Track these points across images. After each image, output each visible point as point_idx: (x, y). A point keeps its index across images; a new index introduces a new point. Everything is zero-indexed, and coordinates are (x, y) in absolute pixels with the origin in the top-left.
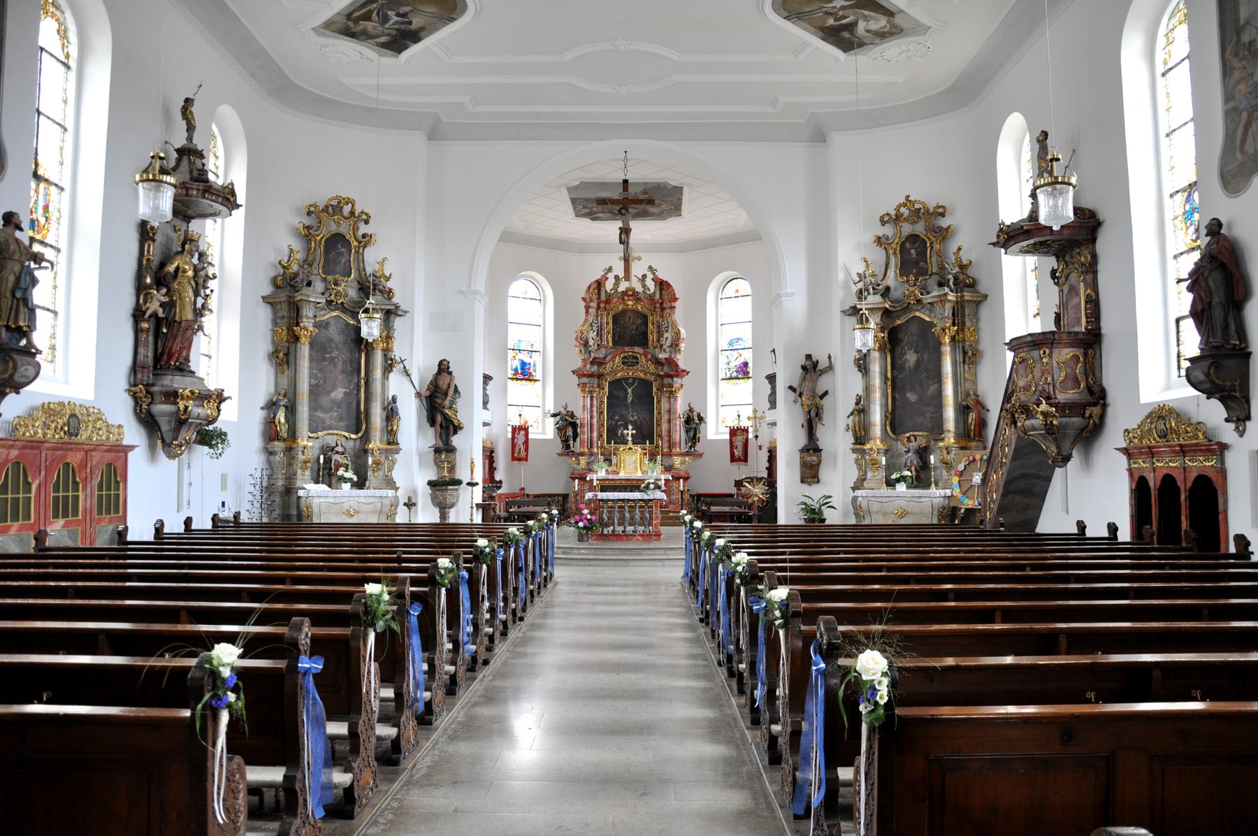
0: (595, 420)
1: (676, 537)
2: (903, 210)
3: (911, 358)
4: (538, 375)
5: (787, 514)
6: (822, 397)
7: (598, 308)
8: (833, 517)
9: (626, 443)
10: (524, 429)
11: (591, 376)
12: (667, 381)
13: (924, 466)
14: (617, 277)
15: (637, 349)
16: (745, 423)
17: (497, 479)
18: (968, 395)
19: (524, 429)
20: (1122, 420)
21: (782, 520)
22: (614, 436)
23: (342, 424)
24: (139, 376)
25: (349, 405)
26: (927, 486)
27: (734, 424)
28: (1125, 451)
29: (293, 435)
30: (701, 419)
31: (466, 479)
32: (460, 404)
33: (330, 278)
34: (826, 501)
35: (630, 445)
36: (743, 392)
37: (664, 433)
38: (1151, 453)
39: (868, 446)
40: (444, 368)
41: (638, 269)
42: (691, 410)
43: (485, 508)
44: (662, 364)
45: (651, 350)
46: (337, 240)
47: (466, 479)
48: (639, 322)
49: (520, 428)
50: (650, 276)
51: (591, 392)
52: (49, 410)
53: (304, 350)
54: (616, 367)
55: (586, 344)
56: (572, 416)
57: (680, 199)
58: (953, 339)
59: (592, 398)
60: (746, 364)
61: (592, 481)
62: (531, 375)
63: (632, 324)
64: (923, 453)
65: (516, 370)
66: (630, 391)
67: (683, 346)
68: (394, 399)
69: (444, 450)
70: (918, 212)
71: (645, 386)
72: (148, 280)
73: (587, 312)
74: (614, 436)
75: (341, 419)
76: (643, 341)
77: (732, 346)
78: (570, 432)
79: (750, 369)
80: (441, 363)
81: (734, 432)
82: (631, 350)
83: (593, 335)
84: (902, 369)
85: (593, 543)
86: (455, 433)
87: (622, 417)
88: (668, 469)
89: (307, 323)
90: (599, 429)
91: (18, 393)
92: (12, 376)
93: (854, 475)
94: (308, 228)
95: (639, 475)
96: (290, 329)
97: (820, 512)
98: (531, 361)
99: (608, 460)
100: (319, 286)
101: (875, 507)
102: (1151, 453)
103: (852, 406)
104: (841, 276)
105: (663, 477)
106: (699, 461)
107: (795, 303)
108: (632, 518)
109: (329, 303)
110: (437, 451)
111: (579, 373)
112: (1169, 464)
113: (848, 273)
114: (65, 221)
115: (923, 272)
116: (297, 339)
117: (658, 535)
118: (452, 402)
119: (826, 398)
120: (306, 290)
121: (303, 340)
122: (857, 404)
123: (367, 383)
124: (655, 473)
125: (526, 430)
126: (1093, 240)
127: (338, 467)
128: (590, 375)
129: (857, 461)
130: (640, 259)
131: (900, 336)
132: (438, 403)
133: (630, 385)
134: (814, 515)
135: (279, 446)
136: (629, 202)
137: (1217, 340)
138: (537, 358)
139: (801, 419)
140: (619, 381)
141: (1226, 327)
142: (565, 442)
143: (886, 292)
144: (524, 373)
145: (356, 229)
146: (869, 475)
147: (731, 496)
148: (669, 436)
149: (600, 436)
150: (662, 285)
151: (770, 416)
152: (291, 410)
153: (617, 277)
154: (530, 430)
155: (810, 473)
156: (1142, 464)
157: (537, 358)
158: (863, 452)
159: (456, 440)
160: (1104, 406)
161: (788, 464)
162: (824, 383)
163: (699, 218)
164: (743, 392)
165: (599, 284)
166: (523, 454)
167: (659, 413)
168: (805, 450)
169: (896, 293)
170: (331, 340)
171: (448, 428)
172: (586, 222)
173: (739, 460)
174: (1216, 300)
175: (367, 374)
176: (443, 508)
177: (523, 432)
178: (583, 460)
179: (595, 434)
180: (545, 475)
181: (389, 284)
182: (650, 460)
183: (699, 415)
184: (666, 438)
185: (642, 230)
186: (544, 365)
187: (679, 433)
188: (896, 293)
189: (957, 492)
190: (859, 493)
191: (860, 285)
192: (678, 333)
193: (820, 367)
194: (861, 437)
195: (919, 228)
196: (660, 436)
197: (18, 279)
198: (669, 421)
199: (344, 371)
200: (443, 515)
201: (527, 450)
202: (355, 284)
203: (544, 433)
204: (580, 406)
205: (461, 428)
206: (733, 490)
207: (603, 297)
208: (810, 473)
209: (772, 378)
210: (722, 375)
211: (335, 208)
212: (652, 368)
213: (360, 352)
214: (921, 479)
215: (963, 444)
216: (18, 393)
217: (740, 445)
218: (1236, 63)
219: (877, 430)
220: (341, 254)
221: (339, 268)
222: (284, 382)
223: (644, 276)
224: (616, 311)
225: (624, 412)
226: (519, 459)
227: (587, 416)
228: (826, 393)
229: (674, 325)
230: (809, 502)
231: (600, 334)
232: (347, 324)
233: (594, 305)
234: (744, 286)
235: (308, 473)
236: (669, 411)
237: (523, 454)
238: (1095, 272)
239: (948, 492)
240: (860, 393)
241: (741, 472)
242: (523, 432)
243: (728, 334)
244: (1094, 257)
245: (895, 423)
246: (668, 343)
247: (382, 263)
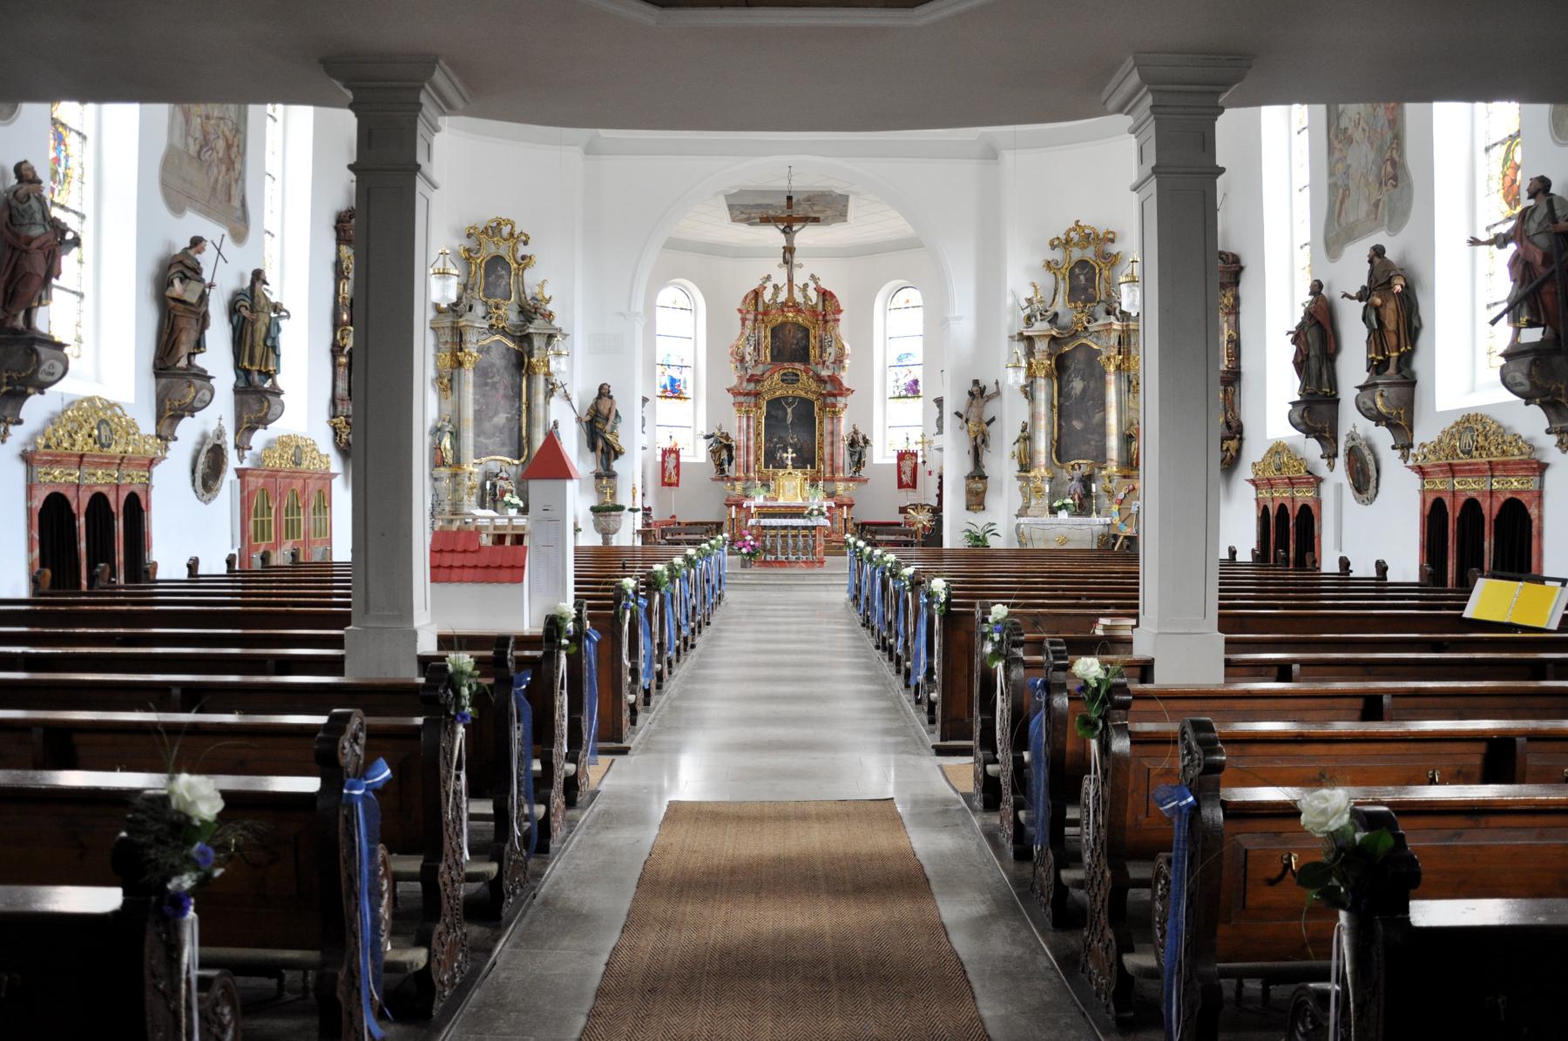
1: (841, 566)
2: (1072, 234)
3: (1077, 385)
4: (688, 392)
5: (952, 539)
6: (988, 424)
8: (995, 543)
9: (785, 467)
10: (674, 452)
11: (748, 394)
12: (830, 400)
13: (1087, 494)
14: (776, 287)
15: (797, 365)
16: (912, 448)
18: (1132, 424)
19: (674, 452)
20: (1254, 452)
21: (947, 544)
22: (772, 460)
23: (505, 449)
24: (340, 408)
25: (511, 429)
26: (1089, 514)
27: (902, 447)
28: (1253, 482)
29: (458, 461)
30: (866, 442)
31: (628, 505)
32: (621, 429)
33: (491, 302)
34: (991, 529)
35: (790, 469)
36: (914, 412)
37: (827, 457)
38: (1270, 484)
39: (1032, 474)
41: (800, 278)
43: (645, 535)
45: (812, 366)
46: (496, 262)
47: (628, 505)
49: (671, 451)
50: (812, 285)
52: (284, 443)
53: (468, 376)
54: (774, 386)
55: (742, 360)
56: (727, 437)
57: (846, 206)
58: (1118, 368)
60: (916, 382)
61: (749, 508)
63: (792, 338)
64: (1087, 481)
67: (847, 362)
68: (556, 424)
69: (605, 474)
70: (1089, 238)
71: (806, 405)
72: (345, 317)
74: (772, 460)
75: (503, 445)
76: (803, 355)
78: (724, 455)
79: (920, 387)
80: (601, 387)
82: (791, 368)
83: (750, 349)
84: (1069, 396)
85: (756, 570)
86: (616, 457)
87: (780, 438)
88: (831, 495)
89: (471, 348)
91: (42, 393)
92: (36, 371)
93: (1018, 502)
94: (469, 250)
95: (799, 501)
96: (453, 355)
97: (985, 539)
98: (681, 377)
99: (766, 485)
100: (480, 310)
101: (1037, 534)
102: (1270, 484)
103: (1018, 433)
104: (1009, 300)
105: (825, 504)
106: (864, 488)
107: (963, 327)
108: (795, 545)
109: (491, 326)
110: (598, 476)
111: (735, 392)
112: (1282, 494)
113: (1016, 300)
114: (89, 178)
115: (1091, 299)
116: (460, 364)
117: (822, 562)
118: (614, 427)
120: (468, 316)
121: (467, 365)
123: (529, 408)
124: (818, 500)
125: (677, 452)
126: (1237, 283)
127: (503, 493)
128: (747, 393)
129: (1021, 488)
130: (801, 266)
131: (1068, 363)
132: (599, 426)
133: (789, 405)
134: (978, 540)
135: (444, 472)
136: (790, 213)
137: (1312, 388)
138: (687, 375)
139: (967, 446)
140: (778, 399)
141: (1320, 376)
143: (1054, 319)
144: (674, 391)
145: (515, 250)
146: (1033, 502)
147: (899, 524)
150: (825, 295)
151: (938, 441)
152: (456, 436)
153: (776, 287)
154: (682, 453)
155: (976, 500)
156: (1265, 494)
158: (1027, 480)
159: (616, 466)
160: (1241, 439)
161: (954, 491)
162: (990, 410)
163: (866, 223)
164: (914, 412)
165: (757, 294)
166: (674, 479)
169: (1064, 319)
170: (492, 365)
172: (744, 227)
173: (908, 486)
174: (1312, 353)
175: (529, 399)
176: (606, 534)
178: (739, 486)
179: (752, 458)
180: (697, 501)
181: (549, 307)
184: (828, 463)
185: (806, 236)
186: (696, 381)
187: (843, 457)
188: (1064, 319)
189: (1116, 519)
190: (1022, 520)
191: (1028, 311)
192: (842, 348)
194: (1026, 466)
195: (1089, 254)
196: (822, 459)
197: (268, 330)
198: (832, 444)
199: (505, 396)
200: (606, 540)
202: (516, 308)
203: (695, 456)
204: (736, 427)
206: (900, 518)
207: (761, 309)
208: (976, 500)
209: (939, 402)
211: (494, 230)
212: (814, 386)
213: (521, 376)
214: (1084, 506)
215: (1126, 472)
216: (42, 393)
218: (1336, 144)
219: (1042, 458)
220: (501, 277)
221: (499, 291)
222: (448, 408)
223: (806, 285)
224: (774, 323)
225: (783, 434)
226: (670, 485)
227: (743, 438)
230: (973, 529)
231: (757, 349)
232: (508, 349)
233: (751, 316)
234: (914, 296)
235: (473, 499)
237: (674, 479)
238: (1237, 314)
239: (1108, 520)
240: (1027, 420)
241: (908, 497)
244: (1237, 299)
245: (1060, 451)
246: (832, 359)
247: (542, 286)
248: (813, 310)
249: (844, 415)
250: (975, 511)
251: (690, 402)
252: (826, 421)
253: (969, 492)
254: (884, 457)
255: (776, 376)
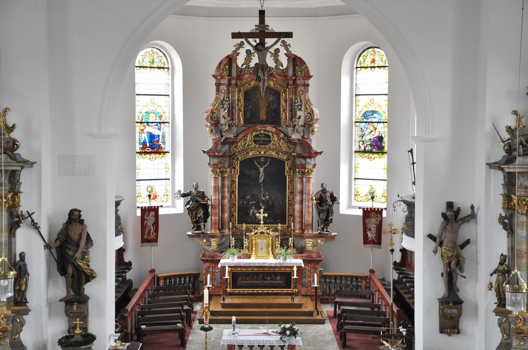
0: (226, 201)
4: (167, 147)
6: (463, 246)
7: (229, 84)
12: (298, 161)
15: (269, 128)
16: (377, 205)
17: (126, 260)
22: (245, 216)
32: (93, 252)
36: (376, 166)
37: (297, 214)
40: (75, 218)
42: (324, 191)
44: (295, 144)
45: (283, 128)
48: (271, 98)
51: (222, 172)
59: (223, 179)
60: (380, 139)
62: (160, 147)
65: (144, 144)
66: (261, 170)
67: (316, 126)
68: (22, 256)
73: (218, 90)
76: (274, 118)
77: (367, 117)
78: (201, 214)
81: (368, 213)
83: (224, 113)
87: (253, 196)
90: (230, 209)
103: (495, 264)
118: (85, 254)
119: (467, 248)
122: (501, 263)
128: (222, 155)
132: (69, 248)
133: (262, 165)
140: (251, 160)
142: (197, 224)
144: (153, 147)
148: (302, 217)
149: (231, 215)
157: (166, 129)
159: (89, 289)
162: (466, 231)
167: (292, 193)
168: (444, 302)
171: (79, 277)
177: (152, 213)
179: (226, 215)
180: (172, 256)
182: (282, 245)
183: (332, 195)
184: (298, 219)
186: (173, 136)
187: (311, 214)
192: (311, 113)
193: (461, 216)
196: (292, 215)
201: (157, 231)
204: (209, 185)
205: (93, 277)
207: (234, 74)
210: (355, 148)
212: (284, 146)
217: (373, 227)
225: (255, 192)
226: (149, 241)
228: (468, 242)
229: (308, 101)
231: (231, 113)
233: (225, 81)
234: (380, 56)
236: (302, 192)
240: (505, 253)
242: (152, 213)
243: (363, 105)
246: (301, 122)
248: (284, 74)
249: (313, 177)
250: (449, 334)
251: (169, 156)
252: (297, 180)
253: (443, 316)
254: (350, 206)
255: (249, 138)
